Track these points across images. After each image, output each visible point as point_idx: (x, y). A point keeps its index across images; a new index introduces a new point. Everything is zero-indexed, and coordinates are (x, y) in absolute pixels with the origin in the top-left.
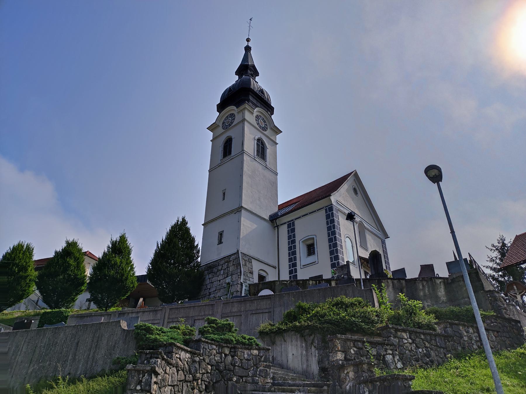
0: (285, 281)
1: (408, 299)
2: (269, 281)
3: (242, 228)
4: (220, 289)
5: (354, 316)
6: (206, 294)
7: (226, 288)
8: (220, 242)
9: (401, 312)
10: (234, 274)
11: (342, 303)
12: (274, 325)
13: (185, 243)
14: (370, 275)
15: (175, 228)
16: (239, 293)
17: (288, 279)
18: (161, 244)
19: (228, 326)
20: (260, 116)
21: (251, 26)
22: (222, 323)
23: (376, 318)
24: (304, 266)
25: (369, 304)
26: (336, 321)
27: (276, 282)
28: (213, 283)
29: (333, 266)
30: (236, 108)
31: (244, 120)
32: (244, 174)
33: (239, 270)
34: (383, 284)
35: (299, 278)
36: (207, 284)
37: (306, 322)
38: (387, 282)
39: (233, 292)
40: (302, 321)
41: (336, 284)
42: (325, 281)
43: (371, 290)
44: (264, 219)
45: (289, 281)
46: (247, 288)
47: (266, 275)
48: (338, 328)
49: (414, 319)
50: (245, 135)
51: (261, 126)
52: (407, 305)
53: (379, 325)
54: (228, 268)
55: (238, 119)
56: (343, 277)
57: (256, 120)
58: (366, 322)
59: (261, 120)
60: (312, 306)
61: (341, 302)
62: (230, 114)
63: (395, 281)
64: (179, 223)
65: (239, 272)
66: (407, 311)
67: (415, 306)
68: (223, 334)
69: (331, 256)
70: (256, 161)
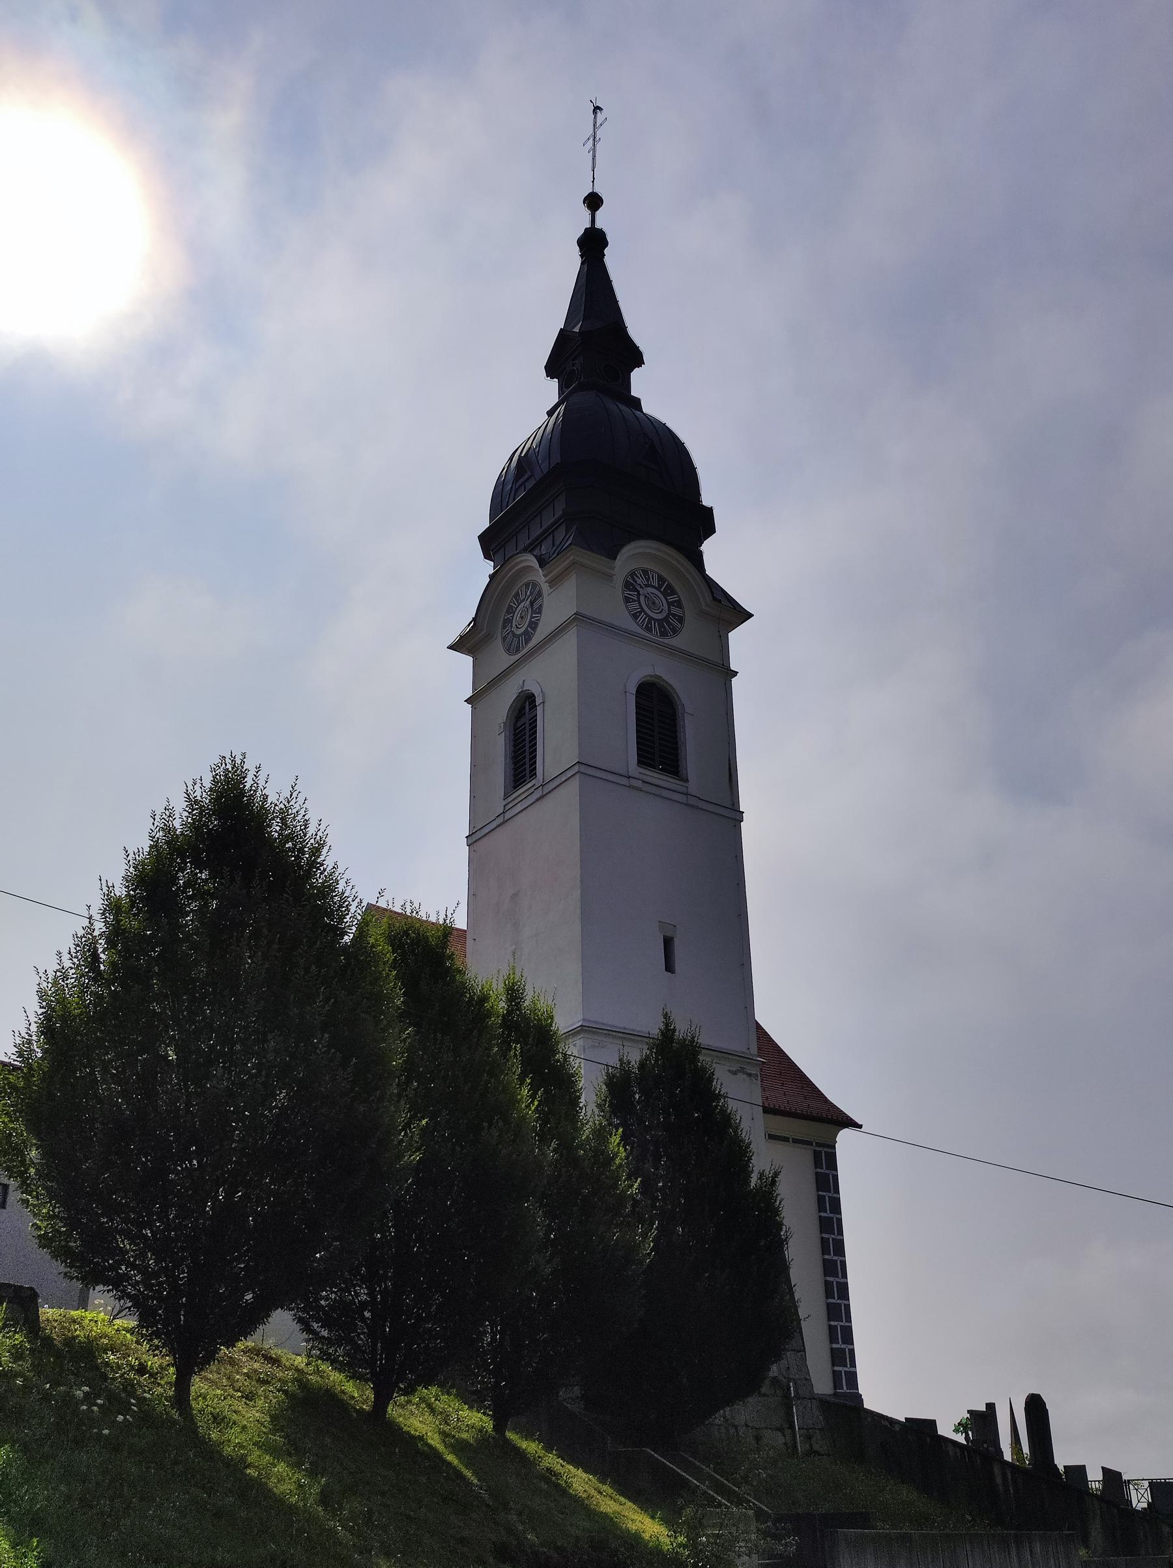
57: (627, 600)
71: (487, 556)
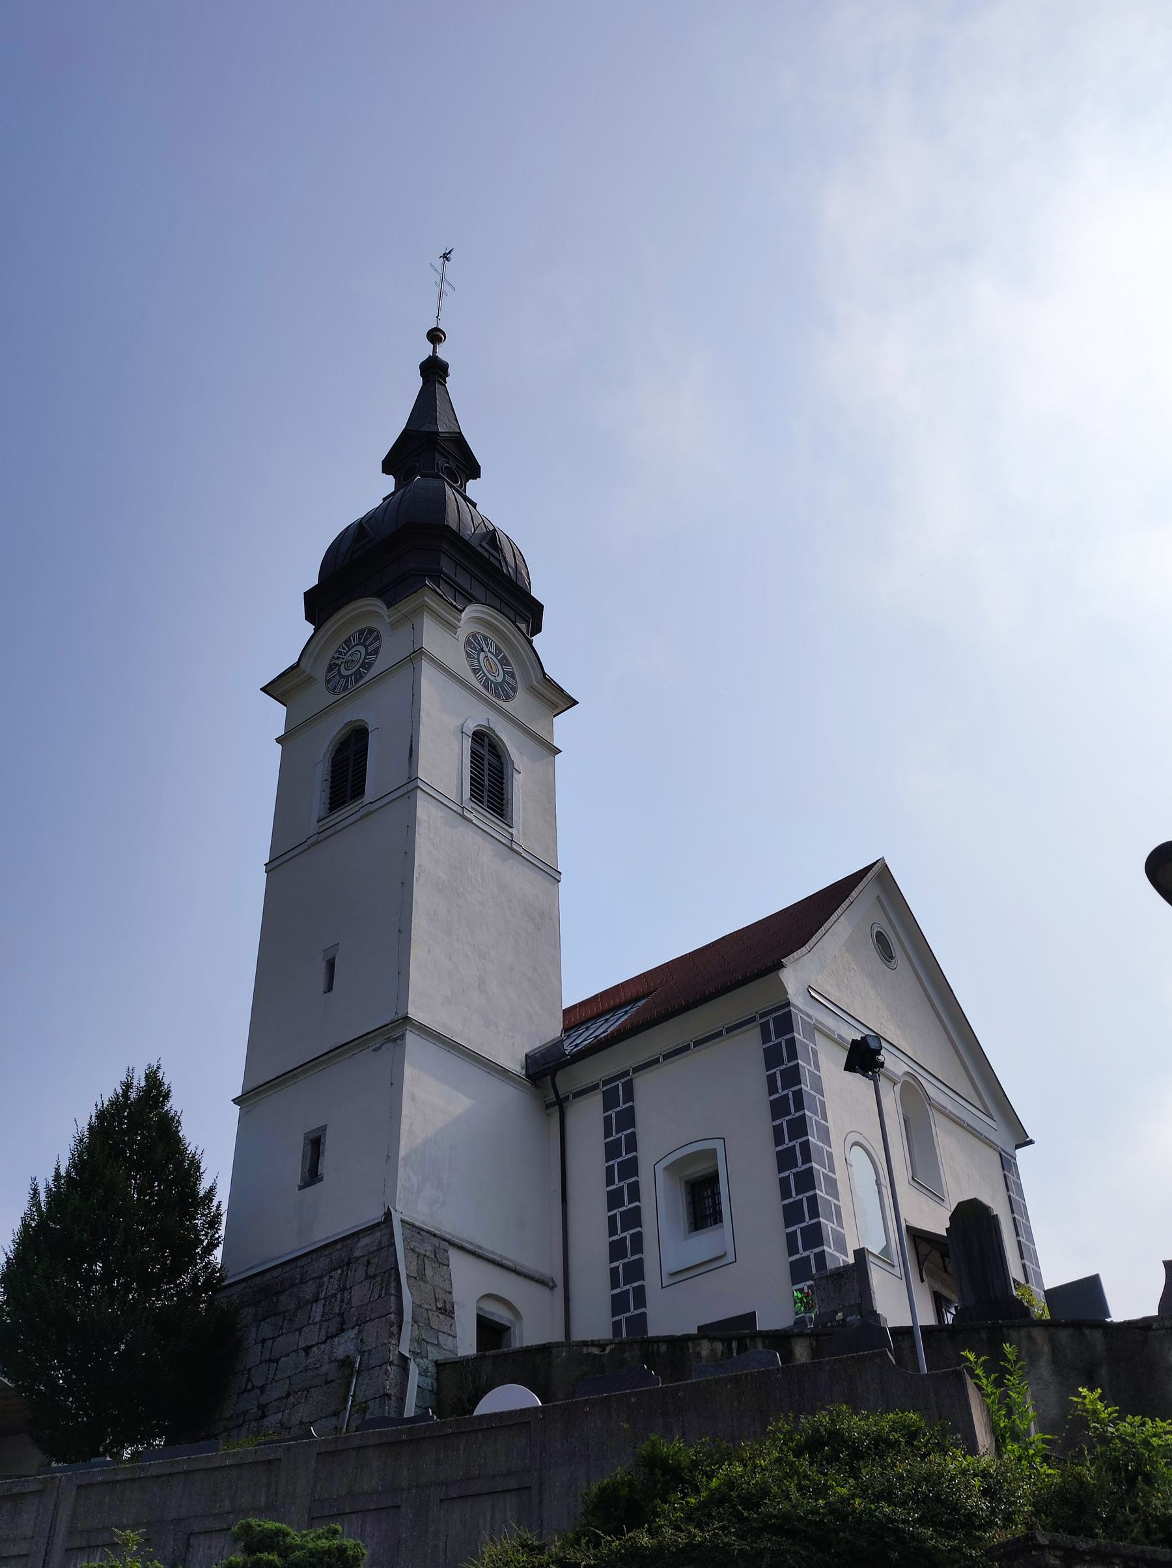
0: (593, 1343)
1: (1116, 1411)
2: (525, 1345)
3: (405, 1111)
4: (307, 1389)
5: (887, 1495)
6: (244, 1413)
7: (334, 1384)
8: (312, 1176)
9: (1088, 1472)
10: (371, 1320)
11: (836, 1438)
12: (541, 1550)
13: (159, 1186)
14: (956, 1308)
15: (113, 1116)
16: (393, 1403)
17: (605, 1334)
18: (48, 1191)
19: (334, 1561)
20: (485, 638)
21: (436, 270)
22: (311, 1545)
23: (985, 1504)
24: (672, 1274)
25: (950, 1439)
26: (810, 1523)
27: (554, 1351)
28: (277, 1361)
29: (798, 1271)
30: (384, 606)
31: (417, 654)
32: (418, 880)
33: (393, 1298)
34: (1007, 1347)
35: (655, 1329)
36: (250, 1370)
37: (682, 1531)
38: (1030, 1338)
39: (366, 1402)
40: (662, 1526)
41: (815, 1353)
42: (767, 1341)
43: (959, 1376)
44: (503, 1072)
45: (611, 1342)
46: (429, 1382)
47: (512, 1318)
48: (819, 1555)
49: (1148, 1504)
50: (422, 714)
51: (488, 679)
52: (1112, 1438)
53: (995, 1537)
54: (346, 1294)
55: (391, 649)
56: (844, 1320)
57: (468, 655)
58: (941, 1524)
59: (489, 655)
60: (709, 1455)
61: (830, 1433)
62: (361, 632)
63: (1064, 1335)
64: (133, 1095)
65: (393, 1309)
66: (1115, 1467)
67: (1149, 1443)
68: (610, 1553)
69: (789, 1230)
70: (471, 821)
71: (309, 617)
